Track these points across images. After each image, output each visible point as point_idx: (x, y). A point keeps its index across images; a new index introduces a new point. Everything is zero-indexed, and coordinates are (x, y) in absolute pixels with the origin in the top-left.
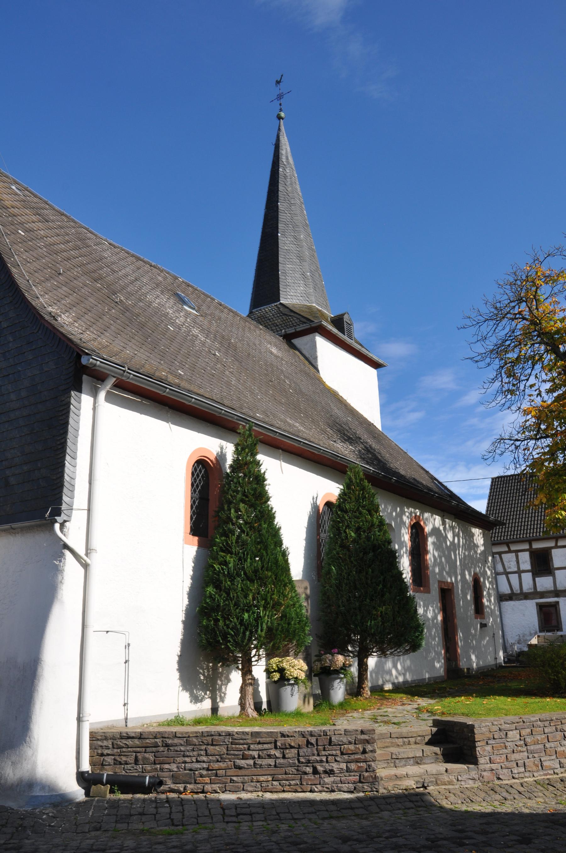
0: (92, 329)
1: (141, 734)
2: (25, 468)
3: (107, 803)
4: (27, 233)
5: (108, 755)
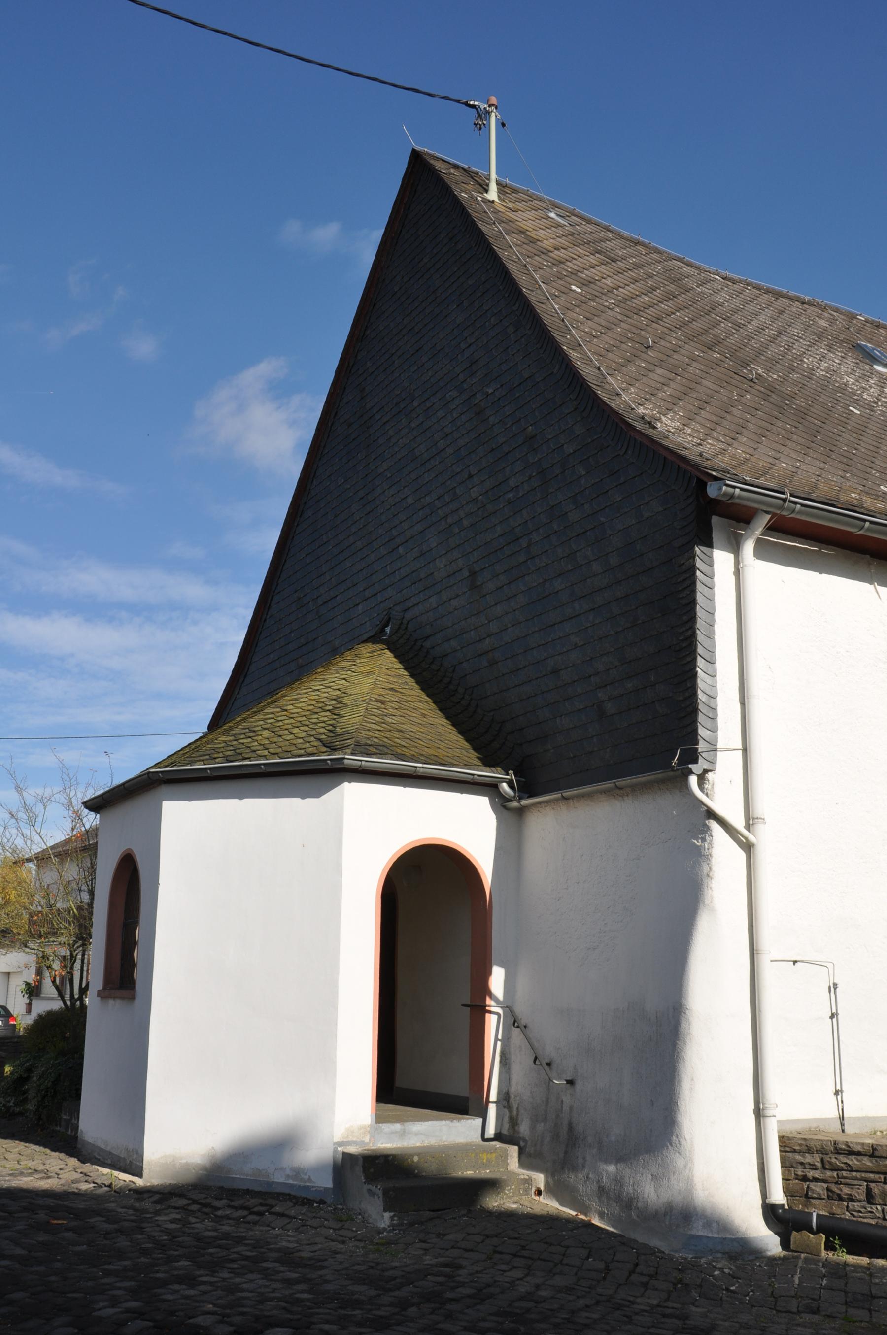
0: (715, 435)
1: (874, 1148)
2: (629, 685)
3: (823, 1267)
4: (585, 288)
5: (816, 1180)
